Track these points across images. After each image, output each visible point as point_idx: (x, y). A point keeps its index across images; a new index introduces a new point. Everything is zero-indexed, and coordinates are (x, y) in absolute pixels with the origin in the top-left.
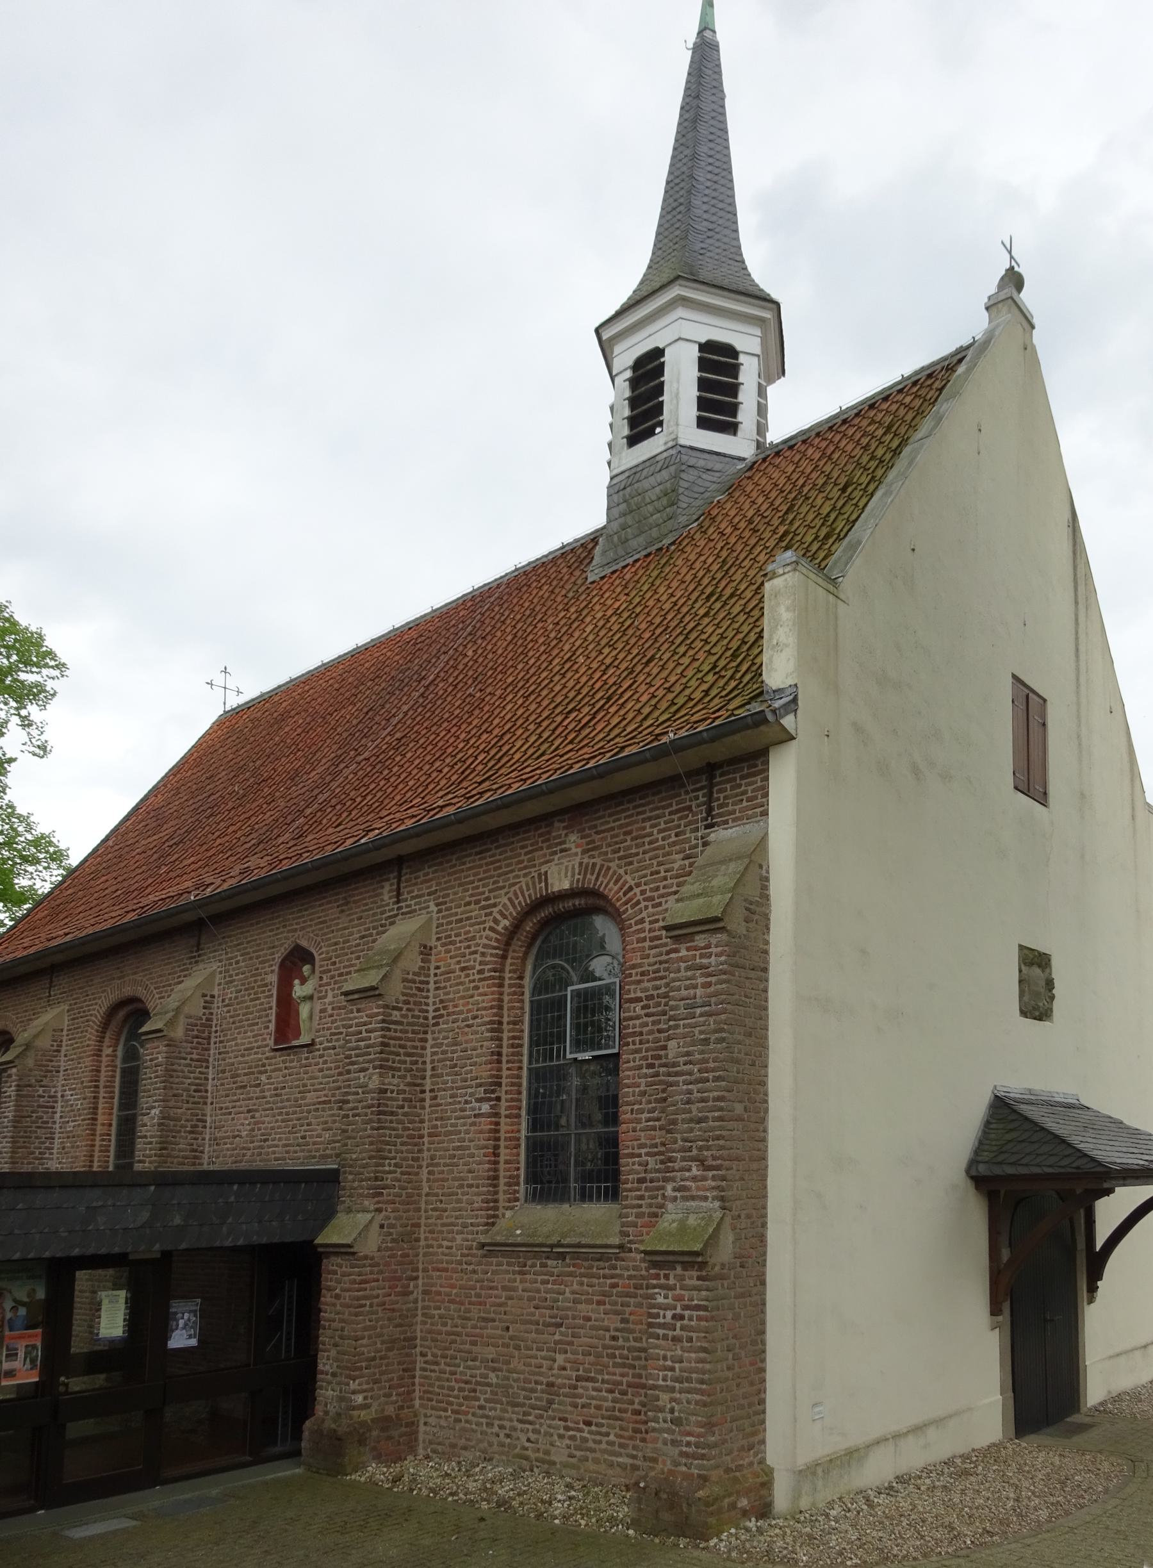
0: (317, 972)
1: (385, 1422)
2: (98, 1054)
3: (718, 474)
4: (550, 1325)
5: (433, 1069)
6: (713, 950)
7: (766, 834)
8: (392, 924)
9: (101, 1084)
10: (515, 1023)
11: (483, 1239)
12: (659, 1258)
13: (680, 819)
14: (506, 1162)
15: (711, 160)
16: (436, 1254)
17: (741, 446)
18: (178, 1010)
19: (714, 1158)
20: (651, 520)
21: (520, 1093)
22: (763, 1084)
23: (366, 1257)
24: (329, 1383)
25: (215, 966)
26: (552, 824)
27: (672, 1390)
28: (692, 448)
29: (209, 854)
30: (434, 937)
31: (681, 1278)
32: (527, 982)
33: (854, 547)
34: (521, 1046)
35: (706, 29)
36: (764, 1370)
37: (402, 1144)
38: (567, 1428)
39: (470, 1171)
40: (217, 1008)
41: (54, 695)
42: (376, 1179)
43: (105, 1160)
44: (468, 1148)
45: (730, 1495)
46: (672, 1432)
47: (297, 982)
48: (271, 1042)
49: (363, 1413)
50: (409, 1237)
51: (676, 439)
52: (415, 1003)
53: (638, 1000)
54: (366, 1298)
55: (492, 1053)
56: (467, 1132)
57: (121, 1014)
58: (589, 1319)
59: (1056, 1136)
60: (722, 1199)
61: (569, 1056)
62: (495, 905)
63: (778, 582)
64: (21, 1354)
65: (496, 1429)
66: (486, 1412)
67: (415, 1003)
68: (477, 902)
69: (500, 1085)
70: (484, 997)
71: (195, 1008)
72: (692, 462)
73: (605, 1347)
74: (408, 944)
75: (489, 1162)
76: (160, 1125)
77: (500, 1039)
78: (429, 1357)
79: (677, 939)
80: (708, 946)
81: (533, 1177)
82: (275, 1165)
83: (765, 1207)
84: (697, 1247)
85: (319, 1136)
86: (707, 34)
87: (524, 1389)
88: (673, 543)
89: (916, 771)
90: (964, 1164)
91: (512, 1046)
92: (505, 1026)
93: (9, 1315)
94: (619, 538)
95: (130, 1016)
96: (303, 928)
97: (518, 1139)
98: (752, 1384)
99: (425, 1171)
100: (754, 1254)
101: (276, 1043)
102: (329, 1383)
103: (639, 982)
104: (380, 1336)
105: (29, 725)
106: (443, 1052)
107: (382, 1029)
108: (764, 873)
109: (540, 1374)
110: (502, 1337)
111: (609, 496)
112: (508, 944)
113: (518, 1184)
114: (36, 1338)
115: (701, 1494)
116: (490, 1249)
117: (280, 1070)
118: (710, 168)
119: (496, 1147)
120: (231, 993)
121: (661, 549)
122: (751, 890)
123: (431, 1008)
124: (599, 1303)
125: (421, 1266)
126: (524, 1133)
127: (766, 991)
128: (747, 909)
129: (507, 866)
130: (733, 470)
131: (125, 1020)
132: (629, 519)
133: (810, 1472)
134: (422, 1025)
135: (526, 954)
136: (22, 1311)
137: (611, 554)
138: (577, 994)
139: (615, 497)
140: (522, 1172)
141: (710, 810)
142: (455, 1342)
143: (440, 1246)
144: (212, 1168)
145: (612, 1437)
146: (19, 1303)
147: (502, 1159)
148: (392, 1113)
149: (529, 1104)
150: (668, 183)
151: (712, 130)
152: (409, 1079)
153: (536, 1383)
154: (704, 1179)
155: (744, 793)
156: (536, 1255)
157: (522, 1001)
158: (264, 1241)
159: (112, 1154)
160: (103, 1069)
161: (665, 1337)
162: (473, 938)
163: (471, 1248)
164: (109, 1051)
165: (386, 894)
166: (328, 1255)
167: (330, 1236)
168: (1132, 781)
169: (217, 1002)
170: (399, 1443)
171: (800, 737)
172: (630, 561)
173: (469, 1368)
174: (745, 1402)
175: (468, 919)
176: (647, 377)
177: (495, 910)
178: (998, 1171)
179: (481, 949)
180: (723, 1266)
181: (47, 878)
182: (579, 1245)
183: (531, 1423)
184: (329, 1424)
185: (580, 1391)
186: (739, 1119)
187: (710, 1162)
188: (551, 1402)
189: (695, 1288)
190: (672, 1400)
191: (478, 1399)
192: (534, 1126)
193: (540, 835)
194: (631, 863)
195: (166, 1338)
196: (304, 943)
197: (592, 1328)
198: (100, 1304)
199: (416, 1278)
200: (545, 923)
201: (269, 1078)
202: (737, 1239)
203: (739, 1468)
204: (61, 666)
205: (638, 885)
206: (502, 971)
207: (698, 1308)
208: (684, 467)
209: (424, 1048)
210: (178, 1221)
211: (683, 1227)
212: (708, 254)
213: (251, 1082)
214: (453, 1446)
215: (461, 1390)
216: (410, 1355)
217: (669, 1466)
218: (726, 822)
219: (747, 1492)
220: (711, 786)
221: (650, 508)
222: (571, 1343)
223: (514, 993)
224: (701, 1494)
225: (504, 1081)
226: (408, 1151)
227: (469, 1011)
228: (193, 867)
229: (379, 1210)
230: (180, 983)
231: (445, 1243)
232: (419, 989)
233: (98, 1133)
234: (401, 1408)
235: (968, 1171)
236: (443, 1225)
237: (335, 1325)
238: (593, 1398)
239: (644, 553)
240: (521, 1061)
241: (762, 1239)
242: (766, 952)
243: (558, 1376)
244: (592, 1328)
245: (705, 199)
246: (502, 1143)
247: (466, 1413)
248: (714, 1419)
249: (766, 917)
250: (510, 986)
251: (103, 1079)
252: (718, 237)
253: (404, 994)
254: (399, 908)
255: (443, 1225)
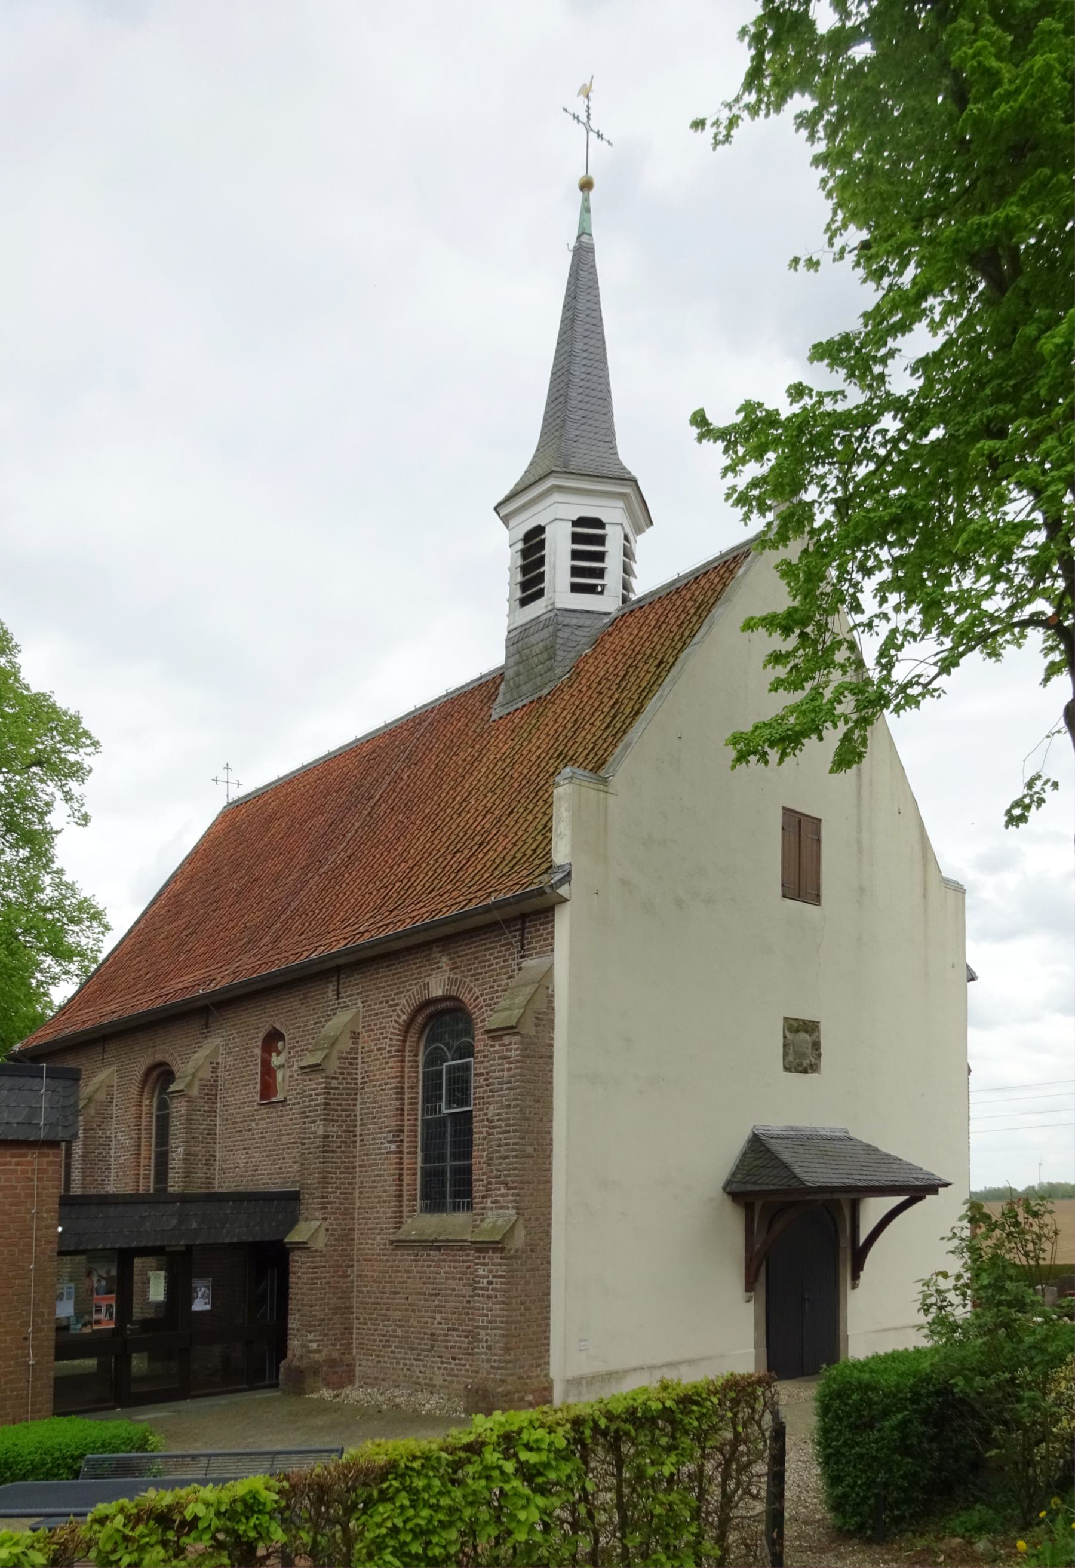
0: (287, 1046)
1: (332, 1363)
2: (139, 1105)
3: (587, 629)
4: (432, 1295)
5: (361, 1120)
6: (513, 1047)
7: (553, 965)
8: (334, 1014)
9: (143, 1127)
10: (412, 1088)
11: (392, 1238)
12: (479, 1246)
13: (506, 950)
14: (408, 1185)
15: (585, 355)
16: (363, 1249)
17: (608, 603)
18: (194, 1075)
19: (513, 1182)
20: (536, 670)
21: (416, 1136)
22: (550, 1133)
23: (316, 1251)
24: (295, 1336)
25: (218, 1041)
26: (431, 949)
27: (486, 1328)
28: (566, 610)
29: (214, 947)
30: (361, 1026)
31: (491, 1258)
32: (421, 1058)
33: (627, 746)
34: (417, 1104)
35: (584, 232)
36: (549, 1318)
37: (341, 1173)
38: (442, 1363)
39: (385, 1192)
40: (222, 1073)
41: (90, 771)
42: (323, 1197)
43: (147, 1185)
44: (383, 1175)
45: (519, 1392)
46: (486, 1354)
47: (274, 1054)
48: (258, 1098)
49: (317, 1355)
50: (346, 1237)
51: (553, 604)
52: (348, 1074)
53: (481, 1074)
54: (316, 1278)
55: (397, 1109)
56: (383, 1164)
57: (155, 1074)
58: (454, 1290)
59: (783, 1163)
60: (517, 1208)
61: (445, 1112)
62: (397, 1004)
63: (560, 790)
64: (104, 1309)
65: (401, 1366)
66: (396, 1355)
67: (348, 1074)
68: (387, 1002)
69: (403, 1131)
70: (392, 1069)
71: (206, 1074)
72: (566, 621)
73: (463, 1308)
74: (342, 1032)
75: (396, 1185)
76: (184, 1159)
77: (402, 1099)
78: (362, 1320)
79: (493, 1038)
80: (510, 1044)
81: (425, 1196)
82: (262, 1188)
83: (550, 1214)
84: (498, 1238)
85: (291, 1167)
86: (585, 238)
87: (417, 1338)
88: (549, 694)
89: (679, 903)
90: (722, 1183)
91: (411, 1104)
92: (406, 1090)
93: (96, 1285)
94: (514, 683)
95: (161, 1076)
96: (277, 1015)
97: (415, 1169)
98: (539, 1326)
99: (357, 1191)
100: (542, 1244)
101: (261, 1099)
102: (295, 1336)
103: (482, 1062)
104: (328, 1304)
105: (71, 799)
106: (368, 1108)
107: (325, 1093)
108: (550, 992)
109: (426, 1328)
110: (404, 1304)
111: (507, 647)
112: (407, 1032)
113: (415, 1200)
114: (112, 1300)
115: (500, 1389)
116: (398, 1245)
117: (264, 1119)
118: (584, 362)
119: (401, 1175)
120: (230, 1061)
121: (540, 698)
122: (540, 1005)
123: (359, 1077)
124: (461, 1279)
125: (355, 1258)
126: (419, 1165)
127: (551, 1071)
128: (537, 1018)
129: (406, 976)
130: (599, 624)
131: (158, 1079)
132: (521, 668)
133: (576, 1382)
134: (353, 1089)
135: (419, 1038)
136: (103, 1283)
137: (509, 696)
138: (449, 1068)
139: (511, 648)
140: (418, 1192)
141: (522, 946)
142: (376, 1309)
143: (367, 1244)
144: (220, 1190)
145: (467, 1367)
146: (101, 1278)
147: (405, 1182)
148: (333, 1152)
149: (422, 1144)
150: (553, 374)
151: (587, 326)
152: (344, 1128)
153: (425, 1334)
154: (507, 1195)
155: (542, 935)
156: (424, 1248)
157: (417, 1072)
158: (250, 1239)
159: (152, 1180)
160: (143, 1116)
161: (483, 1296)
162: (385, 1028)
163: (385, 1245)
164: (147, 1102)
165: (331, 989)
166: (293, 1249)
167: (293, 1237)
168: (925, 865)
169: (221, 1068)
170: (342, 1377)
171: (573, 898)
172: (520, 705)
173: (384, 1326)
174: (534, 1337)
175: (382, 1013)
176: (533, 545)
177: (398, 1008)
178: (750, 1188)
179: (389, 1036)
180: (517, 1251)
181: (90, 935)
182: (448, 1241)
183: (422, 1360)
184: (296, 1363)
185: (449, 1338)
186: (530, 1156)
187: (511, 1185)
188: (433, 1346)
189: (500, 1265)
190: (487, 1334)
191: (390, 1347)
192: (426, 1159)
193: (425, 956)
194: (477, 980)
195: (191, 1304)
196: (278, 1026)
197: (456, 1296)
198: (149, 1279)
199: (352, 1266)
200: (430, 1017)
201: (257, 1125)
202: (528, 1234)
203: (529, 1377)
204: (95, 744)
205: (482, 995)
206: (403, 1051)
207: (500, 1277)
208: (560, 627)
209: (355, 1105)
210: (194, 1225)
211: (494, 1225)
212: (582, 440)
213: (244, 1127)
214: (376, 1379)
215: (381, 1341)
216: (349, 1319)
217: (485, 1375)
218: (531, 955)
219: (533, 1392)
220: (523, 929)
221: (536, 660)
222: (444, 1307)
223: (412, 1067)
224: (500, 1389)
225: (406, 1128)
226: (345, 1178)
227: (383, 1079)
228: (204, 957)
229: (325, 1219)
230: (195, 1052)
231: (370, 1241)
232: (350, 1064)
233: (142, 1164)
234: (343, 1354)
235: (724, 1189)
236: (369, 1229)
237: (299, 1297)
238: (456, 1342)
239: (530, 699)
240: (416, 1115)
241: (548, 1234)
242: (552, 1045)
243: (437, 1329)
244: (456, 1296)
245: (580, 390)
246: (405, 1172)
247: (384, 1356)
248: (510, 1346)
249: (552, 1022)
250: (409, 1061)
251: (144, 1123)
252: (590, 422)
253: (340, 1068)
254: (339, 1003)
255: (369, 1229)
